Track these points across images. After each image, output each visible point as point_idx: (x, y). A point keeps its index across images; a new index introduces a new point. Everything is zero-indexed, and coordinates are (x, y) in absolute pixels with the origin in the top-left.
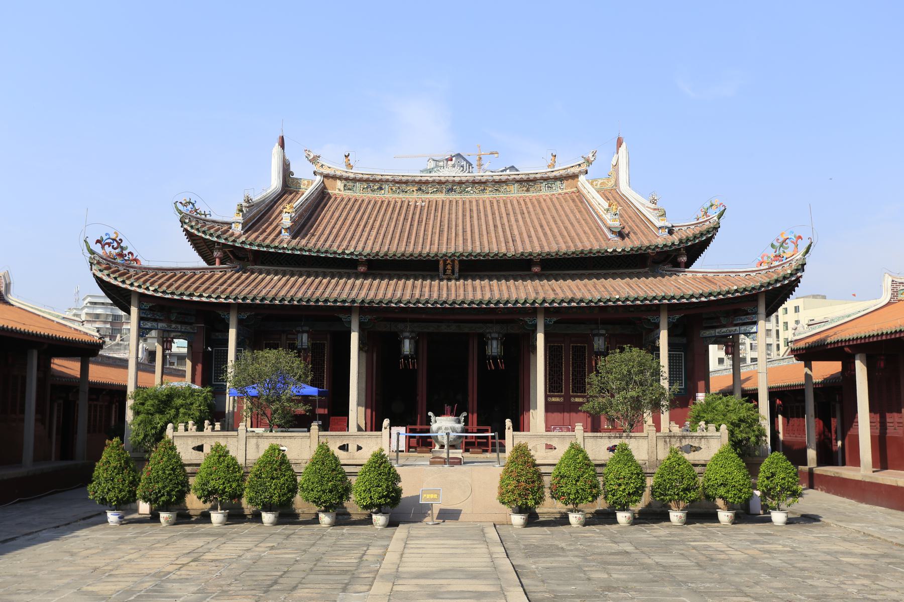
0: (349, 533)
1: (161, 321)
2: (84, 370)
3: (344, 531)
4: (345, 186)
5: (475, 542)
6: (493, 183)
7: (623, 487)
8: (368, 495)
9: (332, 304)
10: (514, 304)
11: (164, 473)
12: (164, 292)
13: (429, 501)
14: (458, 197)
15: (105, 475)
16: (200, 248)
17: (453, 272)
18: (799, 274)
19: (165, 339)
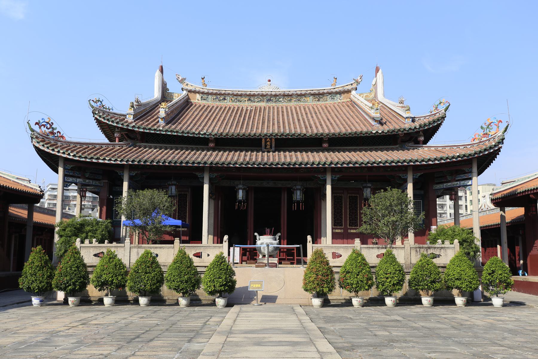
0: (199, 310)
1: (79, 178)
2: (30, 215)
3: (195, 309)
4: (202, 97)
5: (287, 314)
6: (297, 96)
7: (389, 280)
8: (212, 284)
9: (191, 165)
10: (312, 165)
11: (71, 269)
12: (80, 157)
13: (255, 289)
14: (274, 104)
15: (30, 271)
16: (107, 134)
17: (271, 147)
18: (500, 146)
19: (81, 190)
